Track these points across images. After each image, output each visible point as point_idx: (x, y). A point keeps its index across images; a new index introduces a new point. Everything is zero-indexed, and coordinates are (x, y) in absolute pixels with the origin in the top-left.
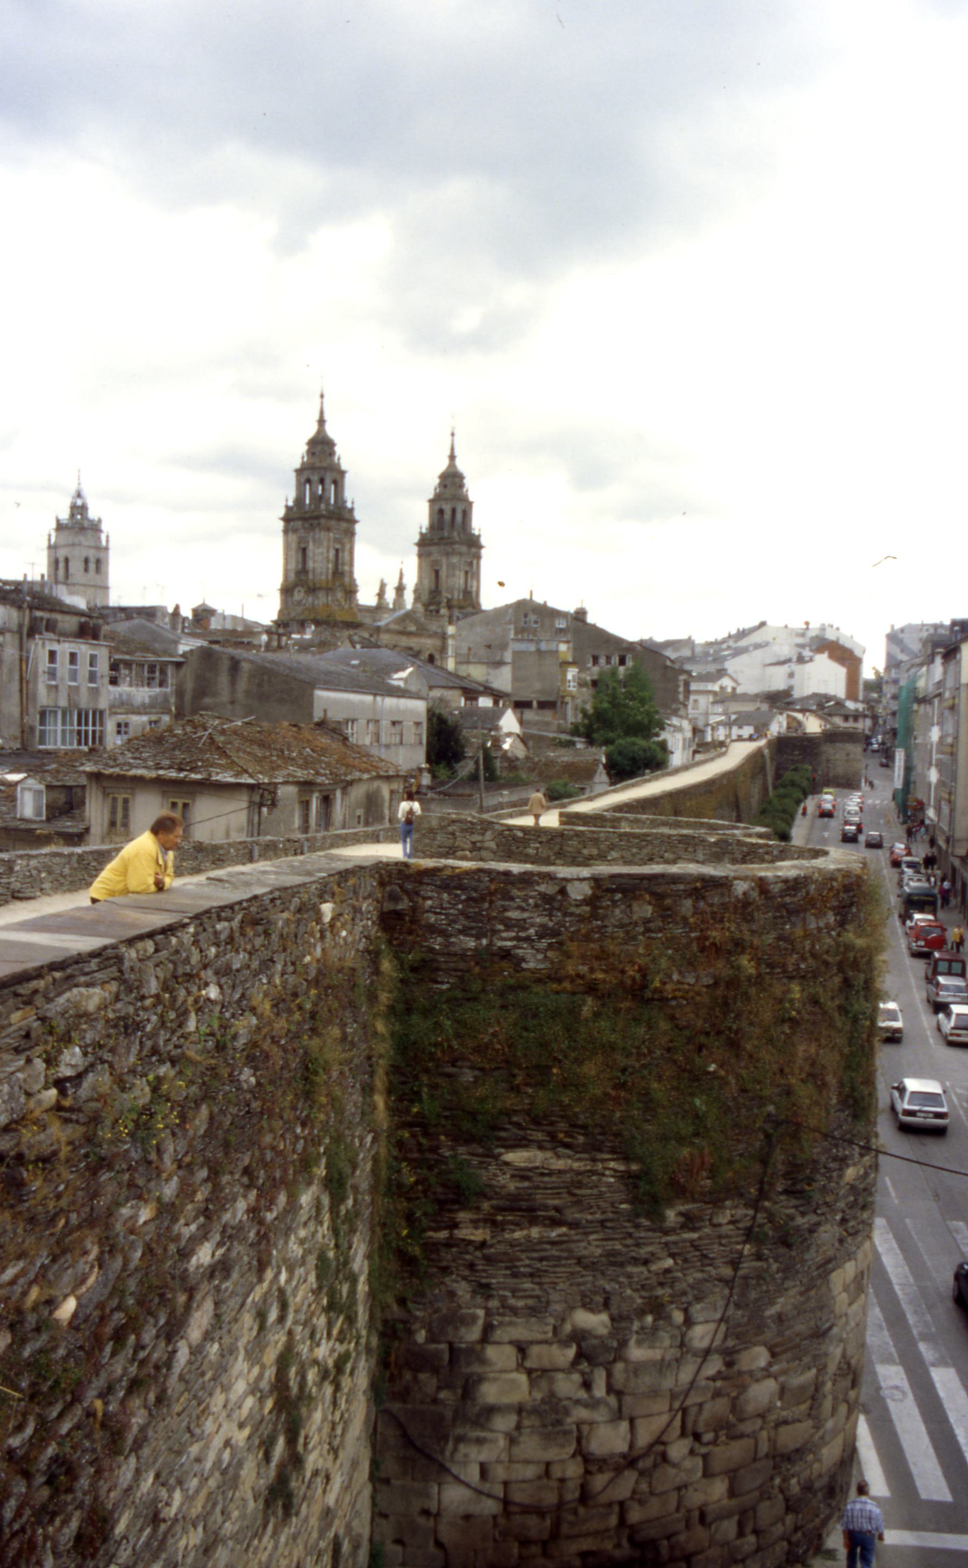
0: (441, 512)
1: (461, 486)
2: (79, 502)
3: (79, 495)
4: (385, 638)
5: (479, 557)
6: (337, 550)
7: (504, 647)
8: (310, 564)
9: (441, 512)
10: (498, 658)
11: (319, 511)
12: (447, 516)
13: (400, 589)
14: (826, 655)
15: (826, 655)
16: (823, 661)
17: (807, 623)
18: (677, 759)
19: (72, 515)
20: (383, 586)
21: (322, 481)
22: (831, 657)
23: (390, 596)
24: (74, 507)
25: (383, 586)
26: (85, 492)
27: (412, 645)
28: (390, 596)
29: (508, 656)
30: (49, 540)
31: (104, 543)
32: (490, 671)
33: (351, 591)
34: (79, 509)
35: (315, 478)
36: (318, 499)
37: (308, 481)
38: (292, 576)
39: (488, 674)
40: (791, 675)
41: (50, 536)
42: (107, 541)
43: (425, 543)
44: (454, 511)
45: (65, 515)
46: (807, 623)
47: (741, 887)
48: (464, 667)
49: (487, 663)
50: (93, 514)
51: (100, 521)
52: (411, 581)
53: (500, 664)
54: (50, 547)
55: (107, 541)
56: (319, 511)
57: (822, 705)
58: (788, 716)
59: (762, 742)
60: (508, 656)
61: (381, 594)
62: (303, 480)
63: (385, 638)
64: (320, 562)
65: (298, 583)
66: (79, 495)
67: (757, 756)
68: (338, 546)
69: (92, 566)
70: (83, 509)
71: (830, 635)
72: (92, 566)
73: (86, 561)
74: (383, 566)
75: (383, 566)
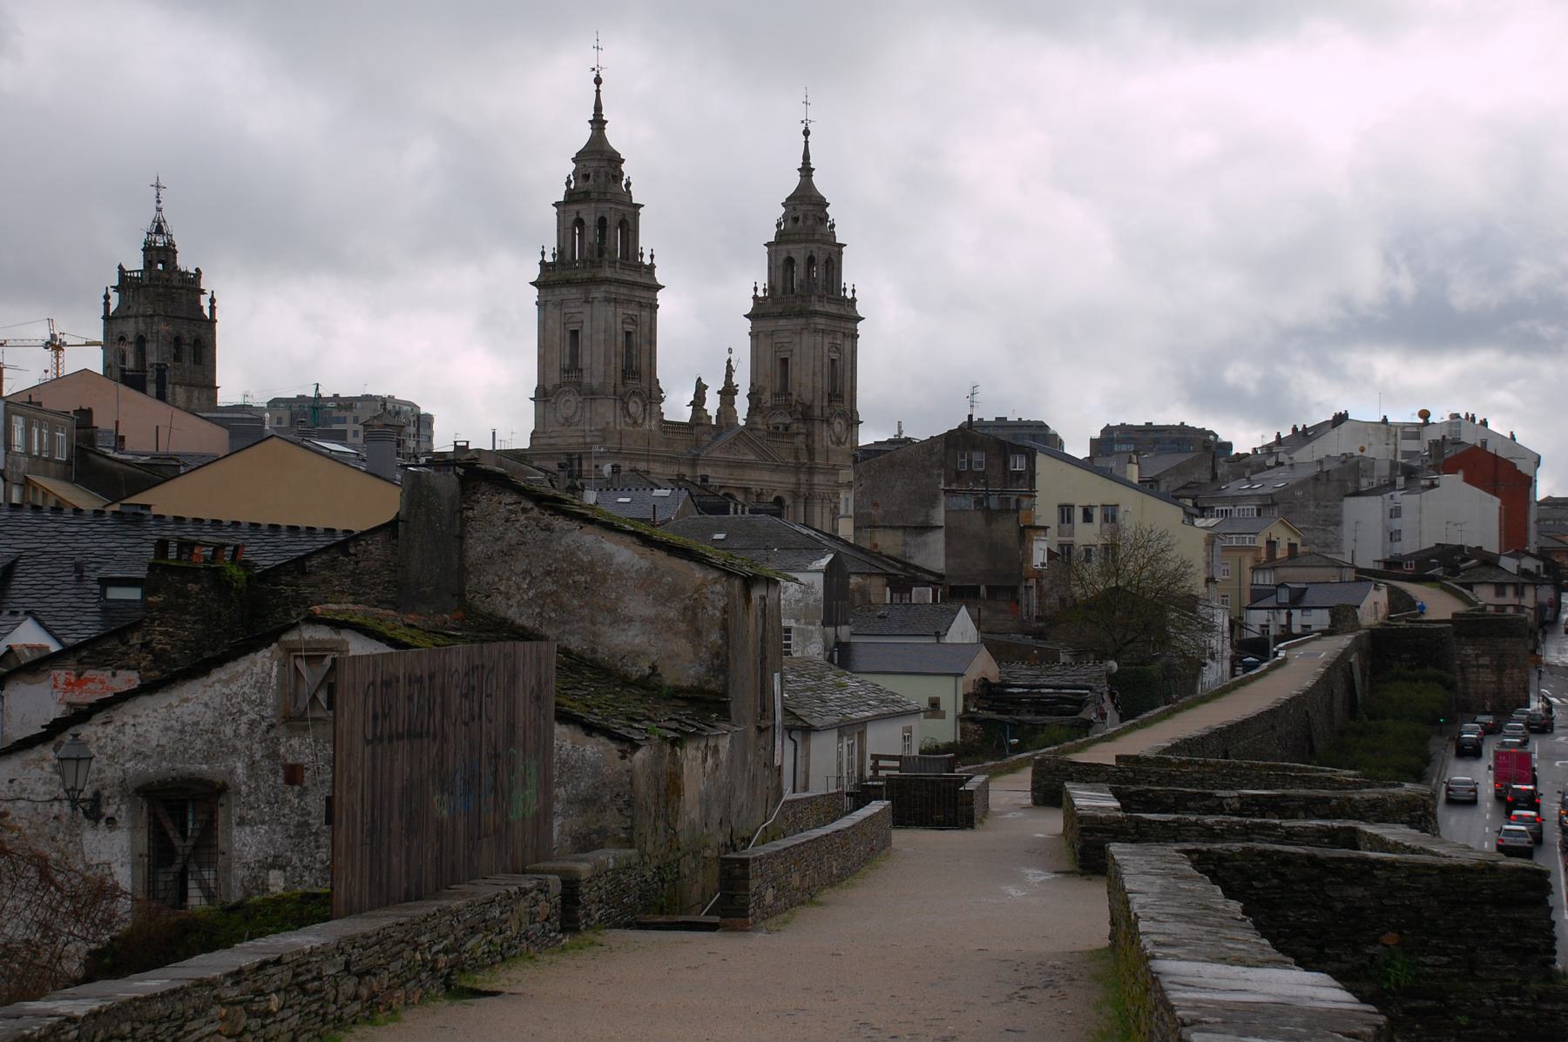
0: (790, 262)
1: (824, 218)
2: (160, 241)
5: (854, 336)
6: (628, 334)
7: (932, 501)
8: (585, 360)
9: (790, 262)
10: (920, 519)
11: (596, 252)
13: (728, 392)
14: (1460, 476)
15: (1460, 476)
16: (1453, 484)
17: (1425, 414)
18: (1214, 673)
19: (149, 263)
20: (701, 389)
22: (1469, 479)
23: (712, 405)
24: (148, 249)
25: (701, 389)
26: (171, 226)
27: (751, 485)
28: (712, 405)
30: (107, 305)
31: (207, 312)
32: (909, 540)
33: (653, 395)
34: (159, 252)
38: (555, 377)
39: (905, 544)
40: (1396, 512)
41: (107, 297)
43: (760, 313)
44: (811, 261)
45: (135, 263)
46: (1425, 414)
47: (1334, 802)
48: (866, 534)
50: (185, 262)
52: (743, 380)
53: (926, 528)
55: (212, 309)
56: (596, 252)
57: (1448, 563)
58: (1393, 591)
59: (1344, 641)
60: (939, 516)
64: (598, 363)
66: (159, 230)
67: (1339, 665)
68: (630, 328)
69: (187, 351)
70: (169, 252)
72: (187, 351)
73: (178, 341)
75: (702, 332)
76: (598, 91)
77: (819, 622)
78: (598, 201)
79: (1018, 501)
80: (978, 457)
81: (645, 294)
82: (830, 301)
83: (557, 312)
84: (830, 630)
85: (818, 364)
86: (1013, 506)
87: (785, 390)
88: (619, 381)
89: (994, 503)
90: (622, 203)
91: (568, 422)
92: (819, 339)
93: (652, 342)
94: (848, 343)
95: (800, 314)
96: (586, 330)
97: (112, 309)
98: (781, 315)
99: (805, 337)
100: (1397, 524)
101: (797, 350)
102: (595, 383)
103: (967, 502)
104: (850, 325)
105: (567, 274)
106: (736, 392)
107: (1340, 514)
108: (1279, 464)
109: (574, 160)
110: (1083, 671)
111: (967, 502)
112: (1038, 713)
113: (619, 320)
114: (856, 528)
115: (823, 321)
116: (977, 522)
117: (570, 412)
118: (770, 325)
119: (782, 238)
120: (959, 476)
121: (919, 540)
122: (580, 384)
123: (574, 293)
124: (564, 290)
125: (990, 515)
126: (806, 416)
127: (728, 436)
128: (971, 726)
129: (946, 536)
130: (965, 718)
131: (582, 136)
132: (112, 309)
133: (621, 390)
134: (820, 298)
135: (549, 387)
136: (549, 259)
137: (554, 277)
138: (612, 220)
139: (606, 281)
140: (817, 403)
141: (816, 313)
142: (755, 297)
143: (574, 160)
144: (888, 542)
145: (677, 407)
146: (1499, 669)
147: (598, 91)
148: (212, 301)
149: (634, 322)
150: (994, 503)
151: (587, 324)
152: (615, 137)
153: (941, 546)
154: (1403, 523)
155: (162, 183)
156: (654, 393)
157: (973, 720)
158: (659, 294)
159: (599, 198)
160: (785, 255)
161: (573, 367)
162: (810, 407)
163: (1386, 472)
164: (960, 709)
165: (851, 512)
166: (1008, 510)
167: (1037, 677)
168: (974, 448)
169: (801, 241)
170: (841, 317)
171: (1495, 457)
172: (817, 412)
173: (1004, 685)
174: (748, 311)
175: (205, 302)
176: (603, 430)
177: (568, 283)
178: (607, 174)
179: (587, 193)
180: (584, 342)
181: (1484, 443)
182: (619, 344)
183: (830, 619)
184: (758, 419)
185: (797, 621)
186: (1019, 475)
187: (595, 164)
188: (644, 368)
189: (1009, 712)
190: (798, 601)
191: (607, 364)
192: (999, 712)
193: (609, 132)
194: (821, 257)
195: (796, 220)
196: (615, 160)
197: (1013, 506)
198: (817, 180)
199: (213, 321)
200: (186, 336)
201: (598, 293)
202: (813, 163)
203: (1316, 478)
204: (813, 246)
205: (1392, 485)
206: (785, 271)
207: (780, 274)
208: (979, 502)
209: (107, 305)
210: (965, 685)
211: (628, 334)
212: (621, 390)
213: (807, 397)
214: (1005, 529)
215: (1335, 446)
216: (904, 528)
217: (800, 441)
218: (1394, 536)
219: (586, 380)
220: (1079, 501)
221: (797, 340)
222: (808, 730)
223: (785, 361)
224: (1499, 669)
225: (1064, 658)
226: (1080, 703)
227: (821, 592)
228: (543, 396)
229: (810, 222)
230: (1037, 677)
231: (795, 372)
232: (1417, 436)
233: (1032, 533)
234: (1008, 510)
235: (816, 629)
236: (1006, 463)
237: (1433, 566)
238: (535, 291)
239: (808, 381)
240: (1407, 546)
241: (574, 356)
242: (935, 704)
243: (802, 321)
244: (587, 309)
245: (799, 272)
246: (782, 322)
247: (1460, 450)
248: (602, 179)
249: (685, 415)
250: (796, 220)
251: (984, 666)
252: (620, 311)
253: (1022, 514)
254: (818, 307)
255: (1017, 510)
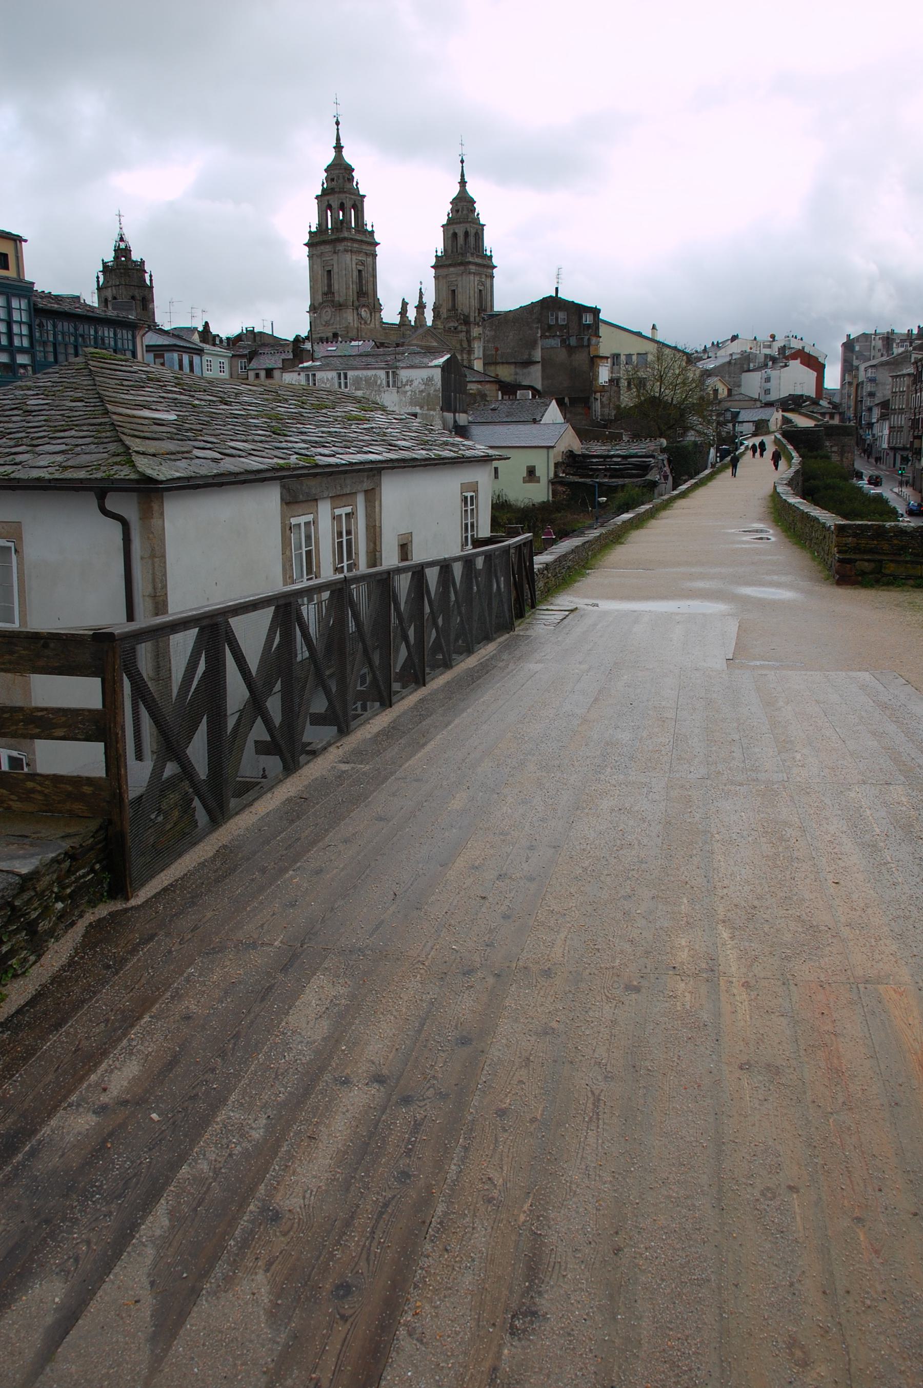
0: (455, 235)
2: (123, 246)
3: (122, 239)
4: (307, 1203)
6: (360, 271)
7: (533, 345)
8: (336, 287)
9: (455, 235)
10: (525, 357)
11: (341, 233)
12: (461, 240)
13: (421, 307)
14: (799, 361)
15: (799, 361)
17: (773, 337)
19: (116, 258)
20: (405, 305)
21: (342, 207)
23: (412, 314)
24: (117, 250)
25: (405, 305)
28: (412, 314)
29: (538, 355)
30: (98, 282)
31: (148, 282)
32: (518, 370)
33: (376, 307)
34: (122, 252)
35: (335, 205)
36: (340, 225)
37: (329, 207)
38: (320, 298)
39: (516, 374)
40: (768, 380)
41: (98, 278)
42: (151, 280)
43: (440, 265)
44: (466, 234)
45: (110, 257)
48: (492, 368)
49: (515, 363)
51: (142, 262)
52: (430, 300)
53: (529, 363)
54: (99, 289)
55: (151, 280)
56: (341, 233)
60: (538, 355)
61: (403, 312)
62: (324, 208)
63: (307, 1203)
64: (344, 288)
65: (324, 299)
66: (122, 239)
68: (360, 268)
71: (796, 345)
74: (405, 274)
75: (405, 274)
76: (338, 129)
77: (438, 408)
78: (340, 192)
79: (589, 339)
80: (562, 315)
81: (369, 248)
82: (478, 256)
83: (319, 260)
84: (449, 416)
85: (472, 292)
86: (585, 343)
87: (454, 308)
88: (355, 299)
89: (573, 341)
90: (353, 194)
91: (327, 324)
92: (472, 277)
93: (374, 276)
94: (488, 280)
95: (461, 264)
96: (335, 269)
97: (101, 283)
98: (450, 265)
99: (464, 277)
100: (768, 385)
101: (460, 285)
102: (341, 300)
103: (555, 342)
104: (490, 271)
105: (324, 238)
106: (425, 307)
107: (740, 381)
108: (709, 357)
109: (451, 203)
110: (643, 446)
111: (555, 342)
112: (611, 477)
113: (354, 263)
114: (485, 364)
115: (474, 267)
116: (562, 355)
117: (328, 318)
118: (444, 271)
119: (450, 222)
120: (550, 327)
121: (525, 371)
122: (333, 301)
123: (327, 248)
124: (322, 247)
125: (571, 350)
126: (466, 321)
127: (420, 331)
128: (560, 488)
129: (543, 370)
130: (555, 482)
131: (455, 190)
132: (101, 283)
133: (356, 303)
134: (472, 254)
135: (316, 305)
136: (439, 254)
137: (316, 240)
138: (348, 204)
139: (344, 239)
140: (472, 314)
141: (470, 263)
142: (436, 256)
143: (326, 171)
144: (506, 373)
145: (390, 315)
146: (842, 453)
147: (338, 129)
148: (151, 276)
149: (363, 264)
150: (573, 341)
151: (335, 266)
152: (471, 190)
153: (539, 374)
154: (772, 385)
155: (122, 213)
156: (377, 306)
157: (562, 483)
158: (377, 248)
159: (340, 189)
160: (452, 232)
161: (329, 292)
162: (468, 317)
163: (762, 360)
164: (552, 475)
165: (481, 356)
166: (583, 346)
167: (609, 451)
168: (560, 309)
169: (460, 223)
170: (484, 266)
171: (809, 354)
172: (472, 319)
173: (584, 456)
174: (433, 264)
175: (147, 277)
176: (347, 327)
177: (324, 242)
178: (344, 177)
179: (333, 189)
180: (335, 276)
181: (803, 348)
182: (354, 277)
183: (448, 406)
184: (439, 323)
185: (421, 407)
186: (589, 326)
187: (337, 172)
188: (370, 292)
189: (591, 476)
190: (422, 391)
191: (347, 288)
192: (582, 476)
193: (345, 153)
194: (472, 232)
195: (457, 211)
196: (349, 170)
197: (585, 343)
198: (469, 188)
199: (151, 287)
200: (137, 295)
201: (341, 247)
202: (343, 143)
203: (729, 363)
204: (468, 225)
205: (766, 365)
206: (453, 242)
207: (450, 242)
208: (563, 341)
209: (98, 282)
210: (556, 456)
211: (360, 271)
212: (356, 303)
213: (466, 311)
214: (580, 358)
215: (735, 348)
216: (515, 363)
217: (462, 336)
218: (767, 392)
219: (337, 299)
220: (624, 352)
221: (460, 279)
222: (150, 491)
223: (454, 291)
224: (842, 453)
225: (625, 438)
226: (645, 468)
227: (439, 383)
228: (313, 309)
229: (465, 212)
230: (609, 451)
231: (460, 298)
232: (770, 347)
233: (598, 360)
234: (583, 346)
235: (436, 414)
236: (580, 318)
237: (790, 405)
238: (307, 249)
239: (467, 302)
240: (773, 397)
241: (330, 285)
242: (531, 471)
243: (462, 268)
244: (335, 257)
245: (461, 240)
246: (452, 269)
247: (793, 351)
248: (341, 181)
249: (396, 320)
250: (457, 211)
251: (570, 441)
252: (354, 257)
253: (592, 349)
254: (471, 259)
255: (588, 346)
